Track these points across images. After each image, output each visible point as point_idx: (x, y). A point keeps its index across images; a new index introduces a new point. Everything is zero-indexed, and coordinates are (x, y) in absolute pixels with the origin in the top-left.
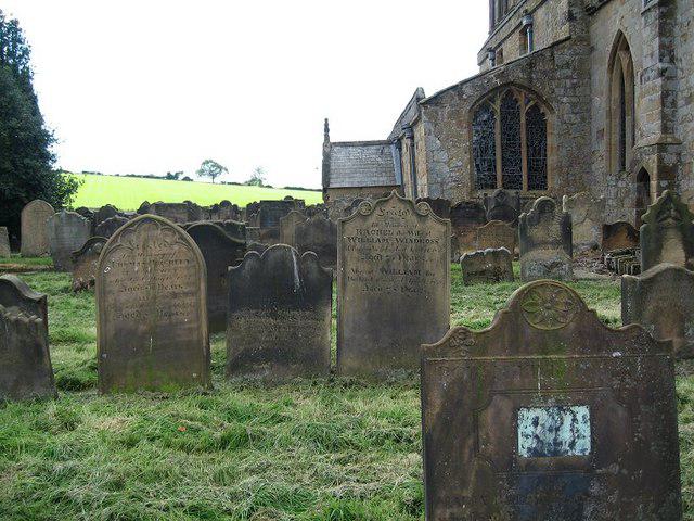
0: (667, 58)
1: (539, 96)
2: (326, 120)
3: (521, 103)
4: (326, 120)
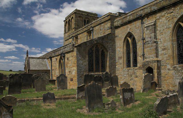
0: (155, 38)
1: (104, 47)
2: (27, 51)
3: (100, 48)
4: (27, 51)
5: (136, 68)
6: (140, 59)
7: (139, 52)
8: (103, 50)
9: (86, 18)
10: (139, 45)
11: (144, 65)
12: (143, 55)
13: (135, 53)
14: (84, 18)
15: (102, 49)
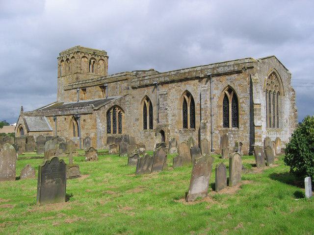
2: (22, 107)
4: (22, 107)
5: (152, 130)
6: (154, 122)
7: (155, 116)
8: (120, 112)
9: (92, 58)
10: (155, 109)
11: (157, 129)
12: (158, 119)
13: (151, 116)
14: (89, 59)
15: (119, 110)
